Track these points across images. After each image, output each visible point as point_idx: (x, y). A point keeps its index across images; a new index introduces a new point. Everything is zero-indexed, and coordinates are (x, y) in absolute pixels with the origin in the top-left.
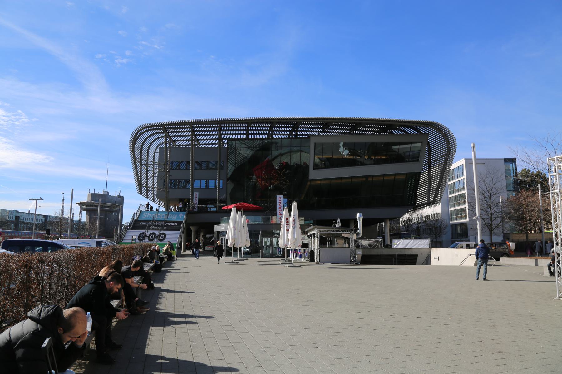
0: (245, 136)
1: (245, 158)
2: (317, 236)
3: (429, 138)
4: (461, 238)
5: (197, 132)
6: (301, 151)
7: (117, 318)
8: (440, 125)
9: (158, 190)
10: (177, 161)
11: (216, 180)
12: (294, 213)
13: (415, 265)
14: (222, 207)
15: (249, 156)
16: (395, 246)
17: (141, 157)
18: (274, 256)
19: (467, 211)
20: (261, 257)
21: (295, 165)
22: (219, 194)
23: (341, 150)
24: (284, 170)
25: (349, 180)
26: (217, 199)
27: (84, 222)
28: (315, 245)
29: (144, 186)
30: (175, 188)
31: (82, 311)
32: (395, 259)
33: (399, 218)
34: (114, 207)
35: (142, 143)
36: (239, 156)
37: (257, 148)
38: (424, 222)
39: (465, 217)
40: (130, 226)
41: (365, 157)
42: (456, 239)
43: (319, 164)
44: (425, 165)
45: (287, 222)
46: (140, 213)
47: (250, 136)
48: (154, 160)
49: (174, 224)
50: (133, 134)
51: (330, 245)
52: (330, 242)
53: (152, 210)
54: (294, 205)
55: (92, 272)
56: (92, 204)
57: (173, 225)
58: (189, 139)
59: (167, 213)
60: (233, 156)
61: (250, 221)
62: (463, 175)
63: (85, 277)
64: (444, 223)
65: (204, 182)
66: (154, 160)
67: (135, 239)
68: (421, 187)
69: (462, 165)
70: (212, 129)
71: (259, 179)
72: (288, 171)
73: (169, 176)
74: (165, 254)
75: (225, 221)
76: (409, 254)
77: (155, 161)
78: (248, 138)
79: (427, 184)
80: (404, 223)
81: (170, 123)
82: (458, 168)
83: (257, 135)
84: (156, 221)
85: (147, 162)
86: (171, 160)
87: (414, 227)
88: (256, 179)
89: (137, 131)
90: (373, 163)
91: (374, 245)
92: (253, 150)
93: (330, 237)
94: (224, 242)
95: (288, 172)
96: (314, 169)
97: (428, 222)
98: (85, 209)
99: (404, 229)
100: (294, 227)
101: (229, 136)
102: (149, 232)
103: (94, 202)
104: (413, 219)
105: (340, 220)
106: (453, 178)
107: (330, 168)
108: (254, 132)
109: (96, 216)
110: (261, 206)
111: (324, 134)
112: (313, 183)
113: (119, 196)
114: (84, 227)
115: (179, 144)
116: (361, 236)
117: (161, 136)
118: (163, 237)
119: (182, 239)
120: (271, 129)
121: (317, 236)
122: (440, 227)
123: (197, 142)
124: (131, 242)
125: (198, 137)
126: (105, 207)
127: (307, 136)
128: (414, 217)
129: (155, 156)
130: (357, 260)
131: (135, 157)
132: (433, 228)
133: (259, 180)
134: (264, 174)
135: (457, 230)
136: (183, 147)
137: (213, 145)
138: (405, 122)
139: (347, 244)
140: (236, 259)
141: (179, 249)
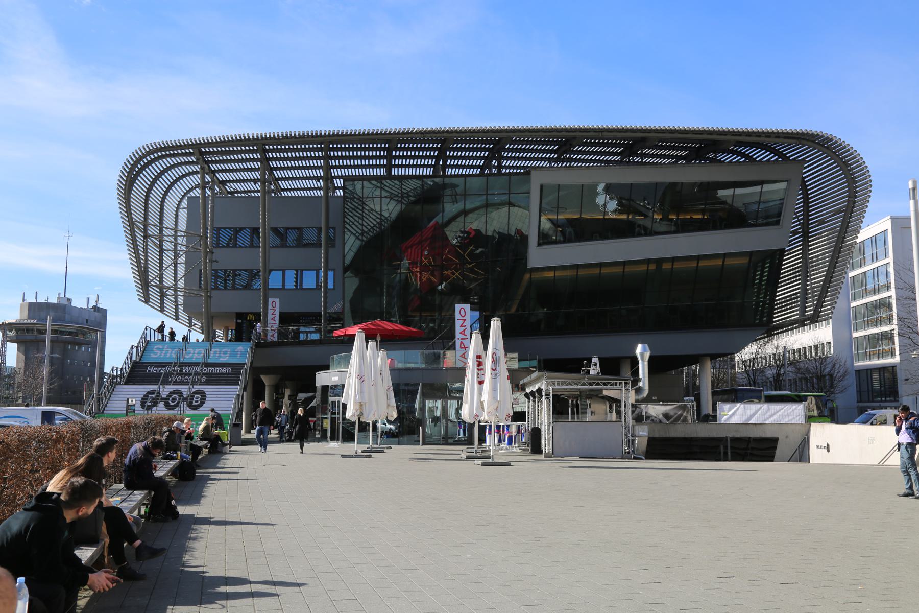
0: (382, 172)
1: (384, 221)
2: (547, 395)
3: (804, 171)
4: (882, 401)
5: (274, 162)
6: (510, 204)
7: (91, 588)
8: (832, 140)
9: (187, 295)
10: (230, 229)
11: (318, 271)
12: (495, 343)
13: (773, 461)
14: (331, 331)
15: (394, 216)
16: (725, 417)
17: (146, 218)
18: (450, 441)
19: (896, 339)
20: (421, 443)
21: (497, 236)
22: (325, 303)
23: (601, 199)
24: (471, 248)
25: (618, 270)
26: (321, 313)
27: (13, 369)
28: (543, 417)
29: (154, 286)
30: (226, 288)
31: (5, 575)
32: (726, 448)
33: (732, 354)
34: (84, 334)
35: (147, 187)
36: (371, 217)
37: (412, 199)
38: (793, 363)
39: (892, 353)
40: (121, 376)
41: (656, 216)
42: (868, 404)
43: (551, 233)
44: (795, 233)
45: (480, 364)
46: (146, 345)
47: (396, 172)
48: (176, 225)
49: (224, 370)
50: (126, 165)
51: (576, 415)
52: (575, 409)
53: (174, 340)
54: (495, 325)
55: (31, 484)
56: (30, 327)
57: (222, 374)
58: (256, 178)
59: (208, 345)
60: (356, 216)
61: (396, 362)
62: (886, 255)
63: (15, 496)
64: (840, 366)
65: (291, 275)
66: (176, 225)
67: (134, 405)
68: (784, 283)
69: (885, 232)
70: (309, 155)
71: (416, 268)
72: (480, 250)
73: (212, 261)
74: (203, 438)
75: (339, 363)
76: (758, 436)
77: (179, 228)
78: (389, 176)
79: (798, 272)
80: (745, 366)
81: (204, 140)
82: (874, 238)
83: (403, 169)
84: (182, 365)
85: (159, 230)
86: (217, 225)
87: (769, 376)
88: (409, 269)
89: (135, 159)
90: (673, 228)
91: (675, 416)
92: (402, 203)
93: (575, 398)
94: (339, 410)
95: (482, 251)
96: (539, 244)
97: (802, 365)
98: (15, 338)
99: (745, 381)
100: (496, 375)
101: (346, 170)
102: (166, 390)
103: (35, 321)
104: (766, 357)
105: (598, 359)
106: (862, 263)
107: (576, 241)
108: (401, 161)
109: (40, 355)
110: (421, 327)
111: (562, 164)
112: (536, 276)
113: (95, 308)
114: (10, 380)
115: (233, 190)
116: (645, 393)
117: (191, 171)
118: (199, 399)
119: (242, 403)
120: (442, 155)
121: (546, 395)
122: (831, 376)
123: (275, 184)
124: (125, 412)
125: (277, 174)
126: (62, 332)
127: (522, 171)
128: (768, 352)
129: (179, 217)
130: (638, 449)
131: (132, 218)
132: (812, 378)
133: (415, 270)
134: (426, 257)
135: (872, 382)
136: (243, 195)
137: (302, 192)
138: (749, 134)
139: (614, 414)
140: (365, 447)
141: (237, 426)
